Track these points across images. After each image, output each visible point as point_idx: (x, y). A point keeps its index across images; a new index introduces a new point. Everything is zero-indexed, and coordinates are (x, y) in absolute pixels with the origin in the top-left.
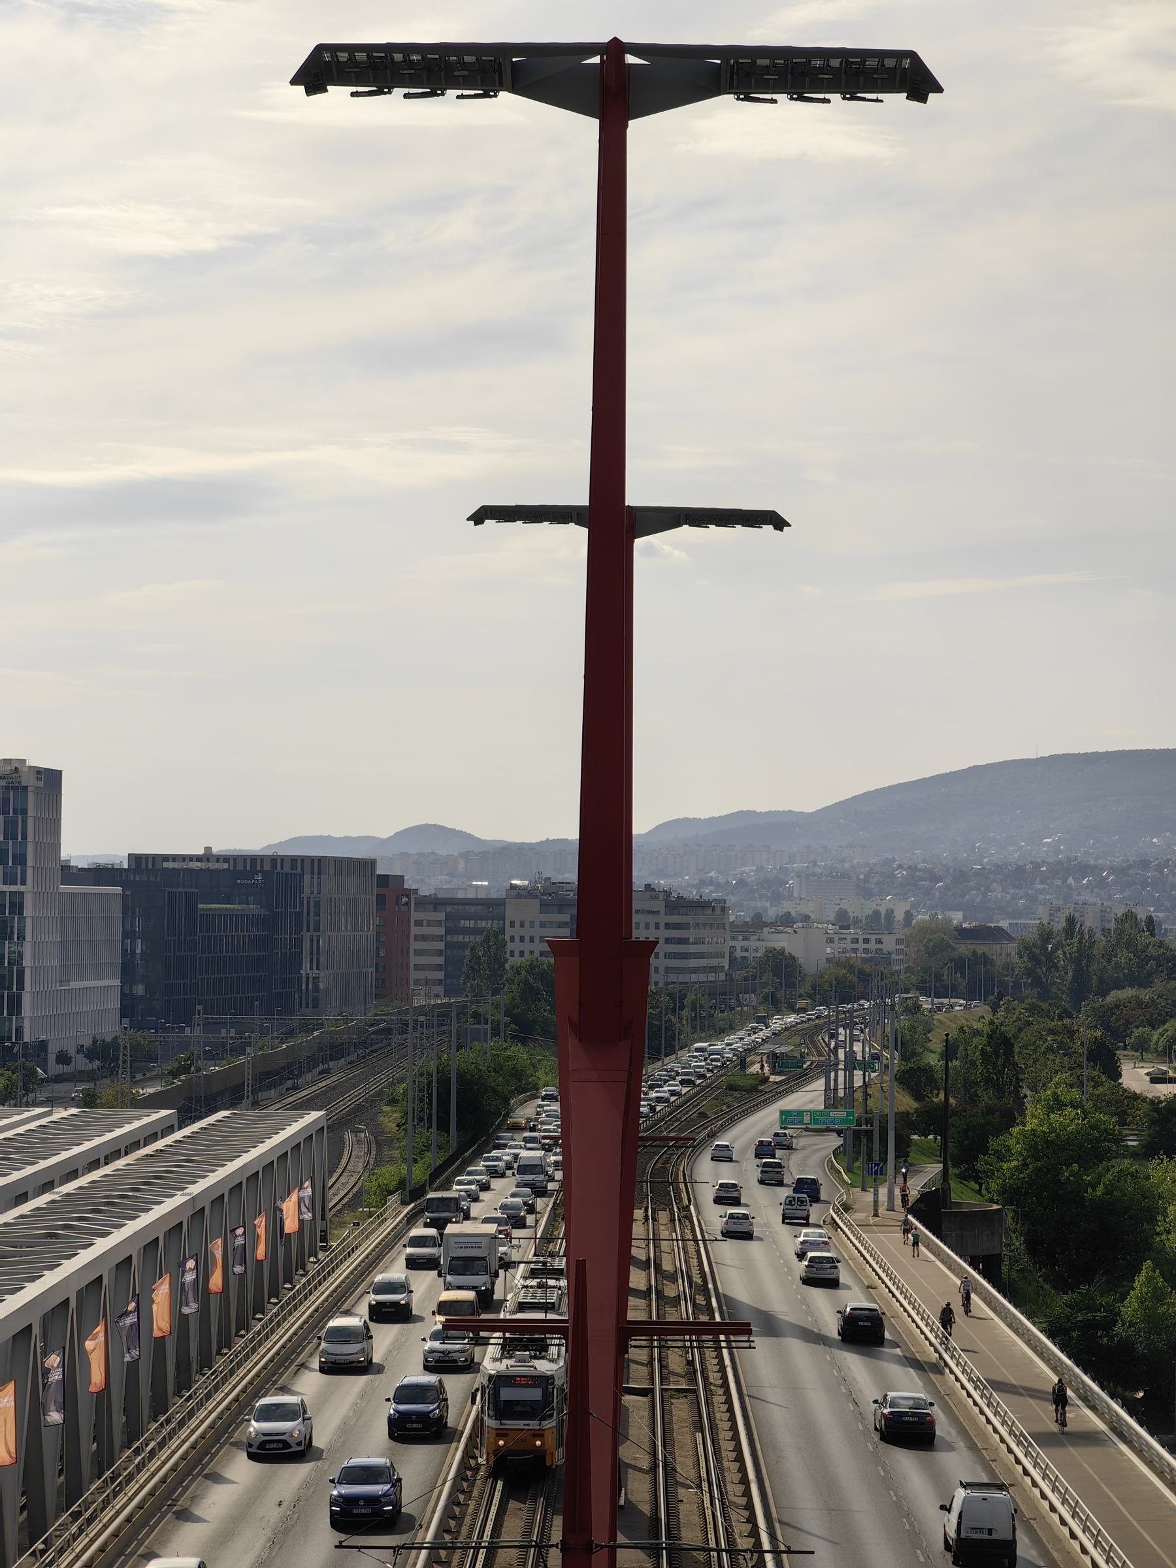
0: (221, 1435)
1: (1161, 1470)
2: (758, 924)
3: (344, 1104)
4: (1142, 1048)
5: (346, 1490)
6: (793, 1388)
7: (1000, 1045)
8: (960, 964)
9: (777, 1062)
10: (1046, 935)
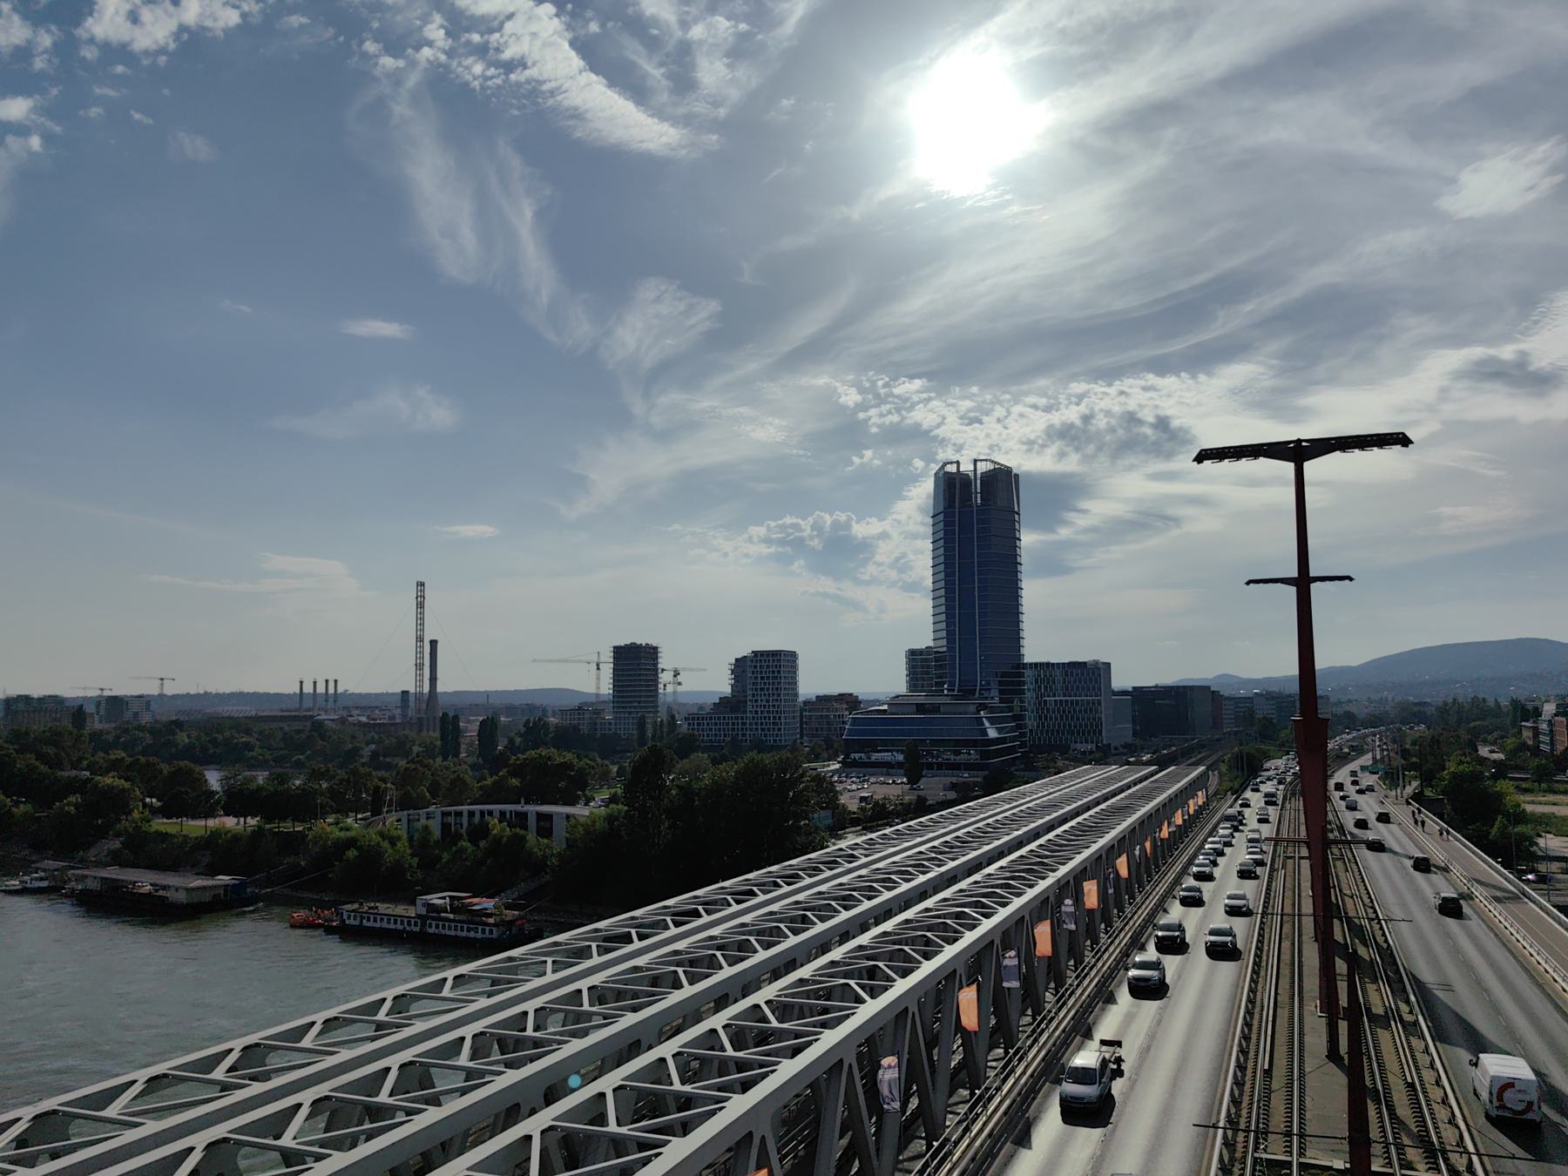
0: (1169, 894)
1: (1560, 923)
2: (1339, 703)
3: (1210, 761)
4: (1485, 742)
5: (1213, 938)
6: (1385, 871)
7: (1435, 742)
8: (1414, 715)
9: (1352, 748)
10: (1446, 704)
